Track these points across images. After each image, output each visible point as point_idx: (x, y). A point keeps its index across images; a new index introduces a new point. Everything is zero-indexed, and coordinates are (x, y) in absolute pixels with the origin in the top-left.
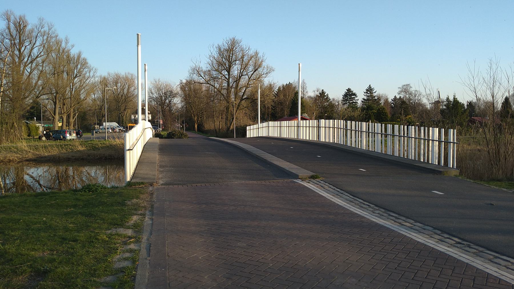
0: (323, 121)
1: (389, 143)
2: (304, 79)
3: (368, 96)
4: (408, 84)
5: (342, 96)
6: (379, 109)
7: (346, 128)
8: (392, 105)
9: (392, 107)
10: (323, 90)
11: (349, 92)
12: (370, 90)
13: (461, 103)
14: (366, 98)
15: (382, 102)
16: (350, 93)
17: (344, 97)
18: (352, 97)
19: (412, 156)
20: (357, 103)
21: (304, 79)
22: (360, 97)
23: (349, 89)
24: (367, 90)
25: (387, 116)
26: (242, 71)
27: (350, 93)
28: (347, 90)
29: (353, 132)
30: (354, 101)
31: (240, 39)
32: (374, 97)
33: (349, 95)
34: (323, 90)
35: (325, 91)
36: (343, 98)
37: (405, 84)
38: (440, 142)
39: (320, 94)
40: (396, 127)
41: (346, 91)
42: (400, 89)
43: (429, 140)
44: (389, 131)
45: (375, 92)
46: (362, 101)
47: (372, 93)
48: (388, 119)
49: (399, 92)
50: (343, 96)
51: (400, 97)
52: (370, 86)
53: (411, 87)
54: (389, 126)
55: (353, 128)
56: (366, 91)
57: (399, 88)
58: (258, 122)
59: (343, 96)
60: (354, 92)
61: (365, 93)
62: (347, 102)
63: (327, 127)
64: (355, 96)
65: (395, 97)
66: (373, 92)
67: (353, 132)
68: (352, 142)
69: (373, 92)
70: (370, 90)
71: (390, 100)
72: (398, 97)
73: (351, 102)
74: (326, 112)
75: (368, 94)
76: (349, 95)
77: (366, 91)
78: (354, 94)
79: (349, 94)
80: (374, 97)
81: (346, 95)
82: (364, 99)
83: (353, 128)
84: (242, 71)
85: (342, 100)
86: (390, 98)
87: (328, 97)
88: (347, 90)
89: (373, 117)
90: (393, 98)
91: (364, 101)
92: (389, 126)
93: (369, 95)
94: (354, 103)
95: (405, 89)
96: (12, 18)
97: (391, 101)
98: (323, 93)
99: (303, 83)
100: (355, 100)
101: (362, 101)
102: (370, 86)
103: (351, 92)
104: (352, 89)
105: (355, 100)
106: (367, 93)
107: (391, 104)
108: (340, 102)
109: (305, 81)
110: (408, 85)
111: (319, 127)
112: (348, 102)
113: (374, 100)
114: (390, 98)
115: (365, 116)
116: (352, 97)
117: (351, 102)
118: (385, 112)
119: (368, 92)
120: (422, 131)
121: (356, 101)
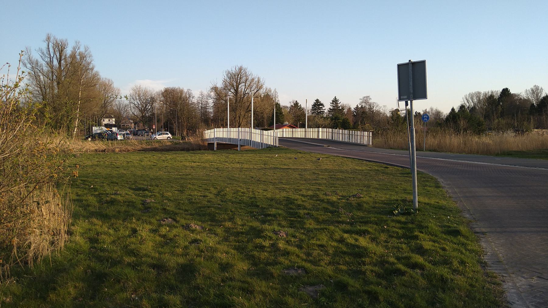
0: (320, 129)
1: (351, 138)
2: (275, 89)
3: (334, 106)
4: (369, 96)
5: (312, 106)
6: (344, 119)
7: (333, 132)
8: (355, 113)
9: (354, 115)
10: (296, 101)
11: (317, 103)
12: (335, 101)
13: (509, 91)
14: (332, 108)
15: (345, 111)
16: (318, 103)
17: (313, 107)
18: (320, 107)
19: (359, 142)
20: (324, 112)
21: (275, 89)
22: (327, 106)
23: (317, 99)
24: (333, 101)
25: (350, 124)
26: (245, 90)
27: (318, 103)
28: (316, 101)
29: (336, 134)
30: (322, 111)
31: (246, 67)
32: (339, 107)
33: (318, 105)
34: (296, 101)
35: (298, 101)
36: (312, 107)
37: (366, 96)
38: (367, 136)
39: (294, 104)
40: (353, 131)
41: (315, 102)
42: (361, 100)
43: (364, 136)
44: (351, 133)
45: (340, 103)
46: (329, 111)
47: (337, 104)
48: (351, 127)
49: (360, 103)
50: (312, 106)
51: (362, 106)
52: (335, 97)
53: (370, 99)
54: (351, 131)
55: (336, 132)
56: (332, 102)
57: (360, 99)
58: (251, 126)
59: (312, 106)
60: (322, 102)
61: (331, 103)
62: (316, 111)
63: (265, 135)
64: (322, 106)
65: (357, 106)
66: (339, 103)
67: (336, 134)
68: (336, 138)
69: (339, 103)
70: (335, 101)
71: (353, 109)
72: (360, 106)
73: (319, 111)
74: (299, 120)
75: (334, 104)
76: (318, 105)
77: (332, 102)
78: (322, 105)
79: (318, 104)
80: (339, 107)
81: (314, 105)
82: (330, 109)
83: (336, 132)
84: (245, 90)
85: (312, 109)
86: (353, 107)
87: (301, 107)
88: (316, 101)
89: (340, 125)
90: (355, 106)
91: (330, 111)
92: (351, 131)
93: (335, 105)
94: (322, 112)
95: (366, 100)
96: (52, 39)
97: (354, 109)
98: (296, 104)
99: (275, 92)
100: (323, 110)
101: (329, 111)
102: (335, 97)
103: (319, 102)
104: (320, 100)
105: (323, 110)
106: (333, 103)
107: (354, 112)
108: (309, 111)
109: (277, 90)
110: (368, 96)
111: (318, 132)
112: (317, 111)
113: (339, 110)
114: (353, 107)
115: (333, 124)
116: (320, 107)
117: (319, 111)
118: (348, 122)
119: (334, 103)
120: (362, 133)
121: (323, 110)
